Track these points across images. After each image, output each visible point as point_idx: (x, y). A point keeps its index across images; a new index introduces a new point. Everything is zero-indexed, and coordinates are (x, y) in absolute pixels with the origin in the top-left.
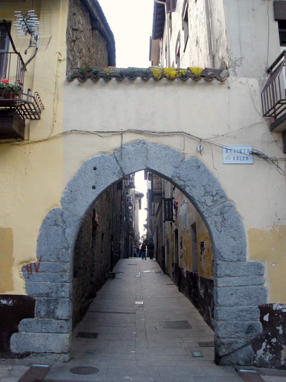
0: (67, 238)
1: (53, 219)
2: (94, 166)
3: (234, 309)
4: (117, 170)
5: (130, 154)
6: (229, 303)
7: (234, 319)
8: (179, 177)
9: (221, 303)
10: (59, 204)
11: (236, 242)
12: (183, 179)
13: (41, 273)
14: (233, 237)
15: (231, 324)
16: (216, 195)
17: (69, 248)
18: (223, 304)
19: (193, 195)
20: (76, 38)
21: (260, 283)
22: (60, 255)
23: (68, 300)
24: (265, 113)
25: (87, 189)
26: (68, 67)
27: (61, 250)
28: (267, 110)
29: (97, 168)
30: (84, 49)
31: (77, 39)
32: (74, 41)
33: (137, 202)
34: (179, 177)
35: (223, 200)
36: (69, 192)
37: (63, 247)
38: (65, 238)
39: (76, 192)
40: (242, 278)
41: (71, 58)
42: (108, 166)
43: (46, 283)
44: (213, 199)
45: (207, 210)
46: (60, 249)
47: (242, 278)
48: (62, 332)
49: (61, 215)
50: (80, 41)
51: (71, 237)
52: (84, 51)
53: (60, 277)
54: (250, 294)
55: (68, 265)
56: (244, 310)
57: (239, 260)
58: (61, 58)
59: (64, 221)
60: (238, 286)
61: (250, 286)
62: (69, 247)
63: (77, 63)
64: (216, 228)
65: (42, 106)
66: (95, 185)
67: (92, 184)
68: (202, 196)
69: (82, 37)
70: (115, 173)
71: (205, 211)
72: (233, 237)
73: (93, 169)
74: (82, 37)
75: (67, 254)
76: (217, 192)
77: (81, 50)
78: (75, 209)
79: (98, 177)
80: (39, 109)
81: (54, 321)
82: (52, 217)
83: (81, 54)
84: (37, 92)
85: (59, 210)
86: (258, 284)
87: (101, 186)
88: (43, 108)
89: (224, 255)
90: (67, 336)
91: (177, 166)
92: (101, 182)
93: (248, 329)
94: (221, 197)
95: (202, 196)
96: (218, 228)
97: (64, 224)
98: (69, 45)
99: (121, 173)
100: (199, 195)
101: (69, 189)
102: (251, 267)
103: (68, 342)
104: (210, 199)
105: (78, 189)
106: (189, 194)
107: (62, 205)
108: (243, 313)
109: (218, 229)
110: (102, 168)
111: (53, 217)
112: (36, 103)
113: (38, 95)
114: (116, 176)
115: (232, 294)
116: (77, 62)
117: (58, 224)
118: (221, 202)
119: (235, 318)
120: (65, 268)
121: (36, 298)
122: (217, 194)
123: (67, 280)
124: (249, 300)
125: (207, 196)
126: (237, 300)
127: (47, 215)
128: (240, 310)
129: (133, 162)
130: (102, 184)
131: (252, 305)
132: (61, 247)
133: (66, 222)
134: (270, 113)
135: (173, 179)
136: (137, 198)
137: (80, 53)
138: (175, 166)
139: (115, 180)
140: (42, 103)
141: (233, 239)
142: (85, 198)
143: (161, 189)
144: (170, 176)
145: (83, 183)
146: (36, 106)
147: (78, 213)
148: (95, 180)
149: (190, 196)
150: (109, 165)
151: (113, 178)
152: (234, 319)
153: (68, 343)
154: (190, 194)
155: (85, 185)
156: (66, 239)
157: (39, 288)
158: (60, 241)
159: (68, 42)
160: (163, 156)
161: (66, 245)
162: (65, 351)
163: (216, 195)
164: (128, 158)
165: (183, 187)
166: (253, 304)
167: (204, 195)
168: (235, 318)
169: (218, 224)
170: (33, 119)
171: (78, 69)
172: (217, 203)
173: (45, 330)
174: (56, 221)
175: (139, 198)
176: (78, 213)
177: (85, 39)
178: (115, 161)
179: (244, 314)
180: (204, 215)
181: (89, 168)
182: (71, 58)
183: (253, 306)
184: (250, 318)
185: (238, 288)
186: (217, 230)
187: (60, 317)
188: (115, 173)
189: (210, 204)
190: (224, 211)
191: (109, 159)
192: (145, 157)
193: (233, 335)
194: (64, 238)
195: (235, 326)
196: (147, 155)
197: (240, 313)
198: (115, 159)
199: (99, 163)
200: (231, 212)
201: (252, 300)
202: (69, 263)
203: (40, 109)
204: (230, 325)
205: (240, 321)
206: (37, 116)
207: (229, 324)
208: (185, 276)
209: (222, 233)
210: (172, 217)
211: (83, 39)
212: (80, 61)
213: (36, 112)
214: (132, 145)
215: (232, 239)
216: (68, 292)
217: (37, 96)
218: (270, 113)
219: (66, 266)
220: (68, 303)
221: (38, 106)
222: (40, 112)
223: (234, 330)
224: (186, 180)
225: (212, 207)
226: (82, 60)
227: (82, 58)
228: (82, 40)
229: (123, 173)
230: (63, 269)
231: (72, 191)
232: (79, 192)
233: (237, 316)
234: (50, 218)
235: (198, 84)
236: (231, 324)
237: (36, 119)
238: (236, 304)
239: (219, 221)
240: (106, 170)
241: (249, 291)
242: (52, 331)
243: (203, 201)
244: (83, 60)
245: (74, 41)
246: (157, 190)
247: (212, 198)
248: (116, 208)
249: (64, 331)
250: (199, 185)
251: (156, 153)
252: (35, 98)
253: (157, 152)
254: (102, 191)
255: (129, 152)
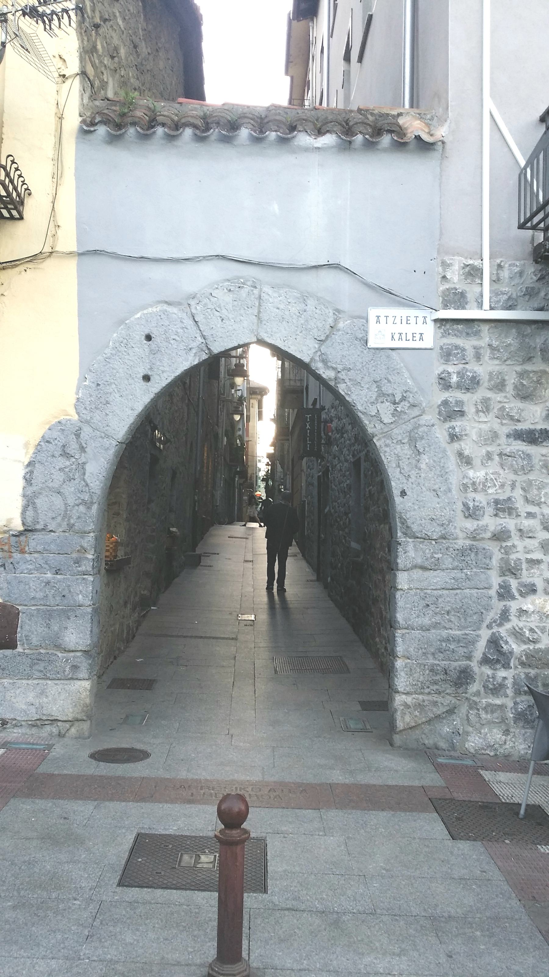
0: (89, 482)
1: (59, 443)
2: (147, 332)
3: (433, 634)
4: (195, 344)
5: (223, 308)
6: (420, 622)
7: (429, 656)
8: (325, 362)
9: (404, 623)
10: (72, 412)
11: (439, 500)
12: (334, 366)
13: (32, 555)
14: (434, 490)
15: (425, 665)
16: (401, 401)
17: (92, 503)
18: (409, 625)
19: (353, 400)
20: (101, 17)
21: (486, 586)
22: (72, 518)
23: (90, 612)
24: (522, 220)
25: (131, 381)
26: (84, 95)
27: (76, 508)
28: (528, 215)
29: (153, 336)
30: (122, 47)
31: (105, 20)
32: (97, 26)
33: (254, 406)
34: (325, 362)
35: (416, 412)
36: (94, 385)
37: (80, 501)
38: (84, 484)
39: (108, 387)
40: (449, 572)
41: (90, 71)
42: (177, 334)
43: (43, 575)
44: (396, 410)
45: (381, 431)
46: (73, 507)
47: (449, 572)
48: (75, 677)
49: (75, 435)
50: (112, 26)
51: (97, 481)
52: (123, 52)
53: (75, 563)
54: (464, 607)
55: (91, 540)
56: (451, 639)
57: (444, 537)
58: (67, 73)
59: (83, 447)
60: (439, 589)
61: (465, 591)
62: (94, 501)
63: (107, 83)
64: (399, 469)
65: (26, 190)
66: (150, 373)
67: (142, 371)
68: (372, 403)
69: (118, 14)
70: (191, 349)
71: (377, 433)
72: (434, 490)
73: (143, 337)
74: (118, 14)
75: (89, 515)
76: (405, 395)
77: (116, 49)
78: (106, 422)
79: (155, 356)
80: (19, 195)
81: (60, 655)
82: (56, 439)
83: (116, 59)
84: (12, 156)
85: (71, 424)
86: (482, 587)
87: (161, 375)
88: (30, 194)
89: (412, 526)
90: (87, 684)
91: (323, 338)
92: (161, 368)
93: (459, 678)
94: (411, 405)
95: (372, 403)
96: (403, 469)
97: (83, 454)
98: (86, 38)
99: (205, 348)
100: (366, 400)
101: (92, 380)
102: (470, 552)
103: (87, 697)
104: (389, 409)
105: (112, 381)
106: (345, 398)
107: (78, 413)
108: (449, 645)
109: (402, 471)
110: (164, 336)
111: (58, 439)
112: (11, 181)
113: (13, 162)
114: (193, 355)
115: (428, 605)
116: (105, 80)
117: (70, 453)
118: (412, 416)
119: (433, 654)
120: (85, 545)
121: (20, 608)
122: (404, 399)
123: (89, 570)
124: (462, 620)
125: (382, 402)
126: (438, 619)
127: (45, 433)
128: (443, 637)
129: (230, 327)
130: (163, 372)
131: (470, 629)
132: (77, 502)
133: (86, 450)
134: (536, 220)
135: (313, 366)
136: (253, 396)
137: (112, 57)
138: (318, 339)
139: (191, 363)
140: (24, 181)
141: (435, 493)
142: (128, 399)
143: (301, 380)
144: (306, 360)
145: (123, 368)
146: (11, 188)
147: (113, 432)
148: (149, 363)
149: (348, 401)
150: (179, 330)
151: (187, 360)
152: (429, 656)
153: (88, 701)
154: (347, 398)
155: (128, 372)
156: (87, 485)
157: (27, 587)
158: (73, 488)
159: (81, 28)
160: (294, 316)
161: (86, 497)
162: (79, 717)
163: (401, 401)
164: (219, 318)
165: (332, 383)
166: (471, 627)
167: (376, 399)
168: (433, 654)
169: (403, 461)
170: (7, 218)
171: (108, 100)
172: (402, 419)
173: (39, 674)
174: (64, 446)
175: (259, 397)
176: (113, 432)
177: (124, 19)
178: (191, 322)
179: (452, 647)
180: (375, 441)
181: (135, 335)
182: (90, 71)
183: (472, 632)
184: (463, 656)
185: (440, 592)
186: (401, 473)
187: (72, 646)
188: (191, 349)
189: (387, 419)
190: (417, 435)
191: (179, 318)
192: (254, 317)
193: (428, 687)
194: (82, 482)
195: (431, 670)
196: (259, 312)
197: (444, 644)
198: (192, 319)
199: (156, 327)
200: (431, 437)
201: (469, 620)
202: (92, 534)
203: (22, 195)
204: (422, 667)
205: (443, 660)
206: (14, 213)
207: (420, 666)
208: (261, 493)
209: (410, 479)
210: (319, 450)
211: (120, 21)
212: (113, 77)
213: (12, 201)
214: (229, 289)
215: (432, 494)
216: (91, 594)
217: (11, 165)
218: (536, 220)
219: (86, 540)
220: (90, 616)
221: (15, 188)
222: (22, 203)
223: (430, 679)
224: (340, 367)
225: (392, 426)
226: (117, 76)
227: (118, 71)
228: (118, 24)
229: (209, 349)
230: (79, 548)
231: (98, 385)
232: (114, 386)
233: (437, 651)
234: (52, 441)
235: (378, 149)
236: (425, 665)
237: (12, 218)
238: (436, 626)
239: (406, 455)
240: (172, 342)
241: (463, 601)
242: (54, 676)
243: (374, 414)
244: (122, 77)
245: (97, 26)
246: (292, 383)
247: (393, 407)
248: (5, 790)
249: (81, 676)
250: (367, 379)
251: (278, 308)
252: (8, 169)
253: (282, 306)
254: (164, 385)
255: (222, 305)
